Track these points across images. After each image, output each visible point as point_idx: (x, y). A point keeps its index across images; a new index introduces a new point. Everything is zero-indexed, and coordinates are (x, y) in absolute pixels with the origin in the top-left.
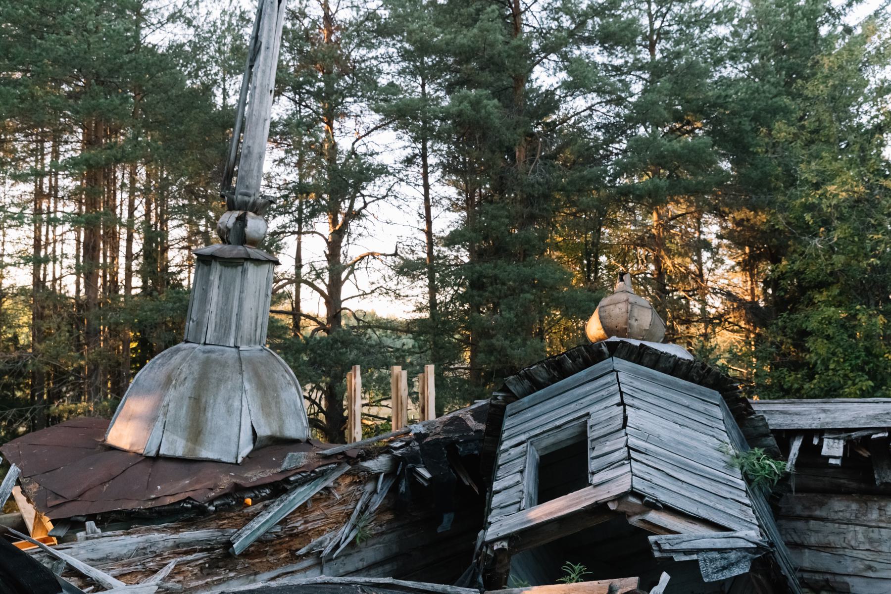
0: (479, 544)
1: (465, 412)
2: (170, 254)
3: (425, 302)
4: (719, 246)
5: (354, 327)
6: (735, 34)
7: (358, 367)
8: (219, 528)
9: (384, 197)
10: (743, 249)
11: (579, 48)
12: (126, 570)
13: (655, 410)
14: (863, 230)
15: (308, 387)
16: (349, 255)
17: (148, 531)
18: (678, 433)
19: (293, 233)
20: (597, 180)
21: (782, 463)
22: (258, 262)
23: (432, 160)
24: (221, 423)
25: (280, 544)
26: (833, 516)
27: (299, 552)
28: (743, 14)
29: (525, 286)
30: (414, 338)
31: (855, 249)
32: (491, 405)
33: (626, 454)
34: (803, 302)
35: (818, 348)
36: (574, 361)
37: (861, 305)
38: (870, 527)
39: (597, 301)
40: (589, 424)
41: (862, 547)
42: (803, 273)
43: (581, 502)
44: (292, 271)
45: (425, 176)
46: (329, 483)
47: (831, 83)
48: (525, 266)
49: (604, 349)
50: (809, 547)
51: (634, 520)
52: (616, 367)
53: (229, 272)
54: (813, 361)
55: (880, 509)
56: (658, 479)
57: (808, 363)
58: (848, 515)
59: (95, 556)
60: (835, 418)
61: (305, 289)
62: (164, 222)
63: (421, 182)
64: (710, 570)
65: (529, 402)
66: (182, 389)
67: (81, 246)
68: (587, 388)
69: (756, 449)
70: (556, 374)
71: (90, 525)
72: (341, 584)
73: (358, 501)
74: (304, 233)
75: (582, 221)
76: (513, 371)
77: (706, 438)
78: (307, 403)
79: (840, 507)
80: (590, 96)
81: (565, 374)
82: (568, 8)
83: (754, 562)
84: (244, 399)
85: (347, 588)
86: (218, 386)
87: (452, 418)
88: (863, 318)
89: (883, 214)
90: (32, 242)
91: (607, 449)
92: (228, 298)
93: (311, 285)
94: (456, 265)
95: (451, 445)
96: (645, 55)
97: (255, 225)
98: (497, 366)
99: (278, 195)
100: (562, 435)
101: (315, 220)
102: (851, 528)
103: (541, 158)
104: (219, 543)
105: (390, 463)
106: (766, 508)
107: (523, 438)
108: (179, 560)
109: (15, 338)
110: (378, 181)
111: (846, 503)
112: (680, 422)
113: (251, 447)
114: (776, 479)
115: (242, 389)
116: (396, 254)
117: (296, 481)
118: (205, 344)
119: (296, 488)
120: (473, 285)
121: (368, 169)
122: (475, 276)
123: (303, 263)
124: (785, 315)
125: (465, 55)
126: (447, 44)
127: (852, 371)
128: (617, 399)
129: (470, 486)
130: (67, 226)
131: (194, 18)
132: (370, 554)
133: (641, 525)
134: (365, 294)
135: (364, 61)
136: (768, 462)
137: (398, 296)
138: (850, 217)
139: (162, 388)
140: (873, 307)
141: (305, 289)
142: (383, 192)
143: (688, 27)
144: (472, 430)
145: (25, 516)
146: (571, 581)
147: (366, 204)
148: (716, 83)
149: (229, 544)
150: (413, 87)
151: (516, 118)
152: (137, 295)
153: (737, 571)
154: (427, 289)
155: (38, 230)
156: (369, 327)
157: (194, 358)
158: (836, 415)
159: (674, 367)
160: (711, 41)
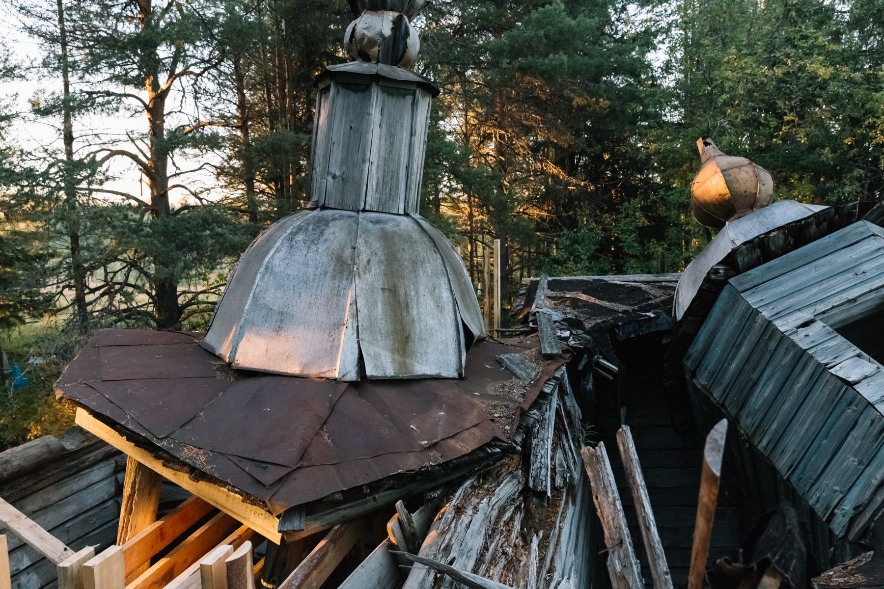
24: (432, 323)
53: (392, 102)
66: (369, 277)
86: (415, 271)
92: (392, 145)
118: (364, 210)
139: (334, 278)
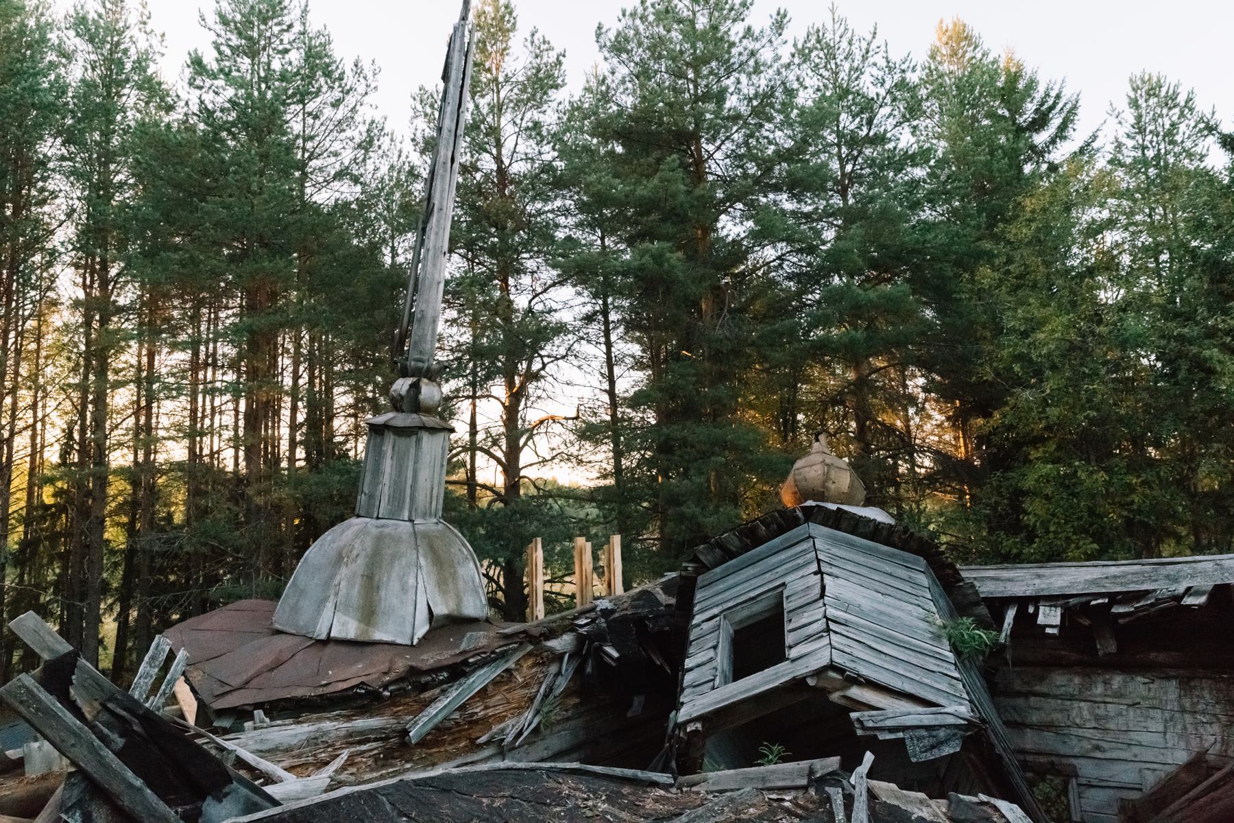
0: (671, 725)
1: (652, 586)
2: (336, 423)
3: (610, 468)
5: (533, 497)
6: (932, 175)
7: (539, 539)
8: (395, 715)
9: (563, 357)
10: (953, 403)
11: (766, 196)
12: (297, 762)
13: (855, 578)
15: (486, 563)
16: (528, 418)
17: (319, 720)
18: (879, 603)
19: (468, 397)
20: (792, 332)
22: (433, 430)
23: (613, 316)
24: (395, 601)
25: (459, 732)
26: (1055, 691)
27: (479, 741)
28: (940, 154)
30: (598, 507)
31: (1071, 401)
33: (824, 626)
35: (1034, 509)
36: (767, 526)
38: (1095, 702)
43: (777, 678)
44: (467, 437)
45: (607, 334)
46: (511, 664)
47: (1034, 226)
49: (799, 514)
50: (1031, 726)
51: (835, 697)
52: (813, 533)
53: (402, 442)
57: (1028, 526)
58: (1071, 690)
59: (264, 747)
61: (481, 458)
62: (329, 391)
63: (602, 340)
66: (353, 567)
67: (241, 416)
68: (782, 556)
70: (748, 541)
71: (259, 714)
72: (525, 770)
73: (541, 683)
74: (479, 397)
76: (705, 540)
77: (911, 607)
78: (485, 581)
79: (1062, 681)
80: (779, 245)
82: (752, 155)
84: (420, 576)
85: (532, 774)
90: (187, 413)
91: (804, 621)
93: (487, 452)
94: (642, 428)
95: (639, 621)
96: (837, 201)
97: (429, 392)
99: (451, 357)
100: (757, 608)
101: (491, 383)
102: (1076, 704)
103: (730, 311)
104: (394, 731)
107: (716, 611)
108: (353, 750)
109: (170, 516)
110: (557, 341)
112: (883, 591)
113: (426, 628)
114: (988, 650)
115: (418, 566)
116: (577, 418)
117: (475, 663)
118: (378, 518)
119: (474, 671)
121: (546, 328)
122: (663, 438)
123: (478, 428)
125: (647, 206)
126: (627, 196)
127: (1074, 533)
128: (814, 567)
129: (661, 666)
130: (228, 397)
131: (362, 175)
132: (555, 742)
133: (843, 702)
134: (545, 461)
135: (540, 215)
141: (481, 458)
142: (562, 351)
143: (881, 170)
145: (185, 708)
146: (770, 762)
147: (544, 365)
148: (914, 226)
149: (405, 732)
150: (592, 239)
151: (701, 271)
152: (301, 468)
153: (947, 750)
154: (611, 454)
155: (194, 401)
156: (551, 496)
157: (368, 533)
158: (1052, 580)
159: (874, 532)
160: (906, 183)
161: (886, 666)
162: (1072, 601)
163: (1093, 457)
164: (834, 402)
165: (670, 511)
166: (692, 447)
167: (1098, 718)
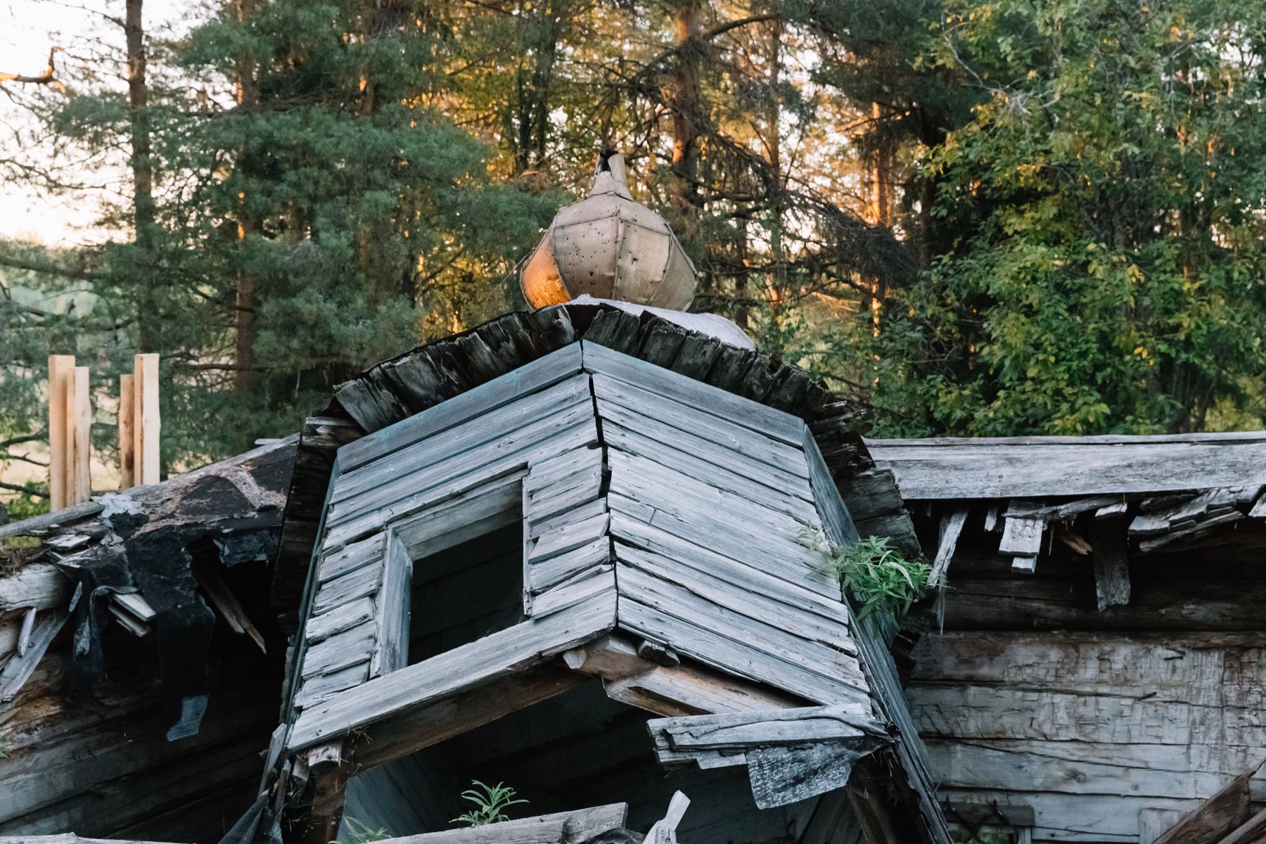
0: (274, 754)
4: (817, 100)
10: (867, 110)
13: (668, 457)
14: (1113, 79)
18: (716, 507)
21: (923, 567)
26: (1013, 675)
29: (378, 174)
30: (99, 292)
31: (1095, 121)
32: (302, 448)
33: (606, 552)
34: (983, 233)
36: (496, 347)
37: (1096, 242)
38: (1080, 694)
39: (546, 217)
40: (527, 486)
41: (1064, 735)
42: (987, 168)
43: (506, 655)
48: (376, 125)
50: (964, 741)
51: (618, 691)
52: (590, 363)
54: (995, 361)
55: (1101, 659)
56: (671, 601)
57: (986, 366)
58: (1041, 673)
60: (1029, 475)
64: (770, 785)
65: (390, 441)
69: (873, 538)
70: (453, 376)
75: (513, 22)
81: (473, 377)
83: (857, 765)
87: (201, 480)
88: (1098, 269)
89: (1153, 47)
98: (306, 363)
100: (465, 514)
102: (1046, 698)
105: (51, 586)
106: (885, 662)
107: (376, 520)
111: (1038, 649)
114: (909, 599)
120: (248, 165)
122: (256, 142)
124: (946, 259)
127: (1071, 383)
128: (590, 433)
133: (633, 700)
136: (894, 565)
137: (54, 186)
138: (1088, 51)
140: (1120, 249)
144: (252, 507)
146: (482, 819)
153: (823, 786)
154: (130, 172)
158: (1034, 469)
161: (721, 629)
162: (1064, 510)
163: (1119, 237)
164: (634, 89)
165: (267, 308)
166: (324, 165)
167: (1080, 722)
